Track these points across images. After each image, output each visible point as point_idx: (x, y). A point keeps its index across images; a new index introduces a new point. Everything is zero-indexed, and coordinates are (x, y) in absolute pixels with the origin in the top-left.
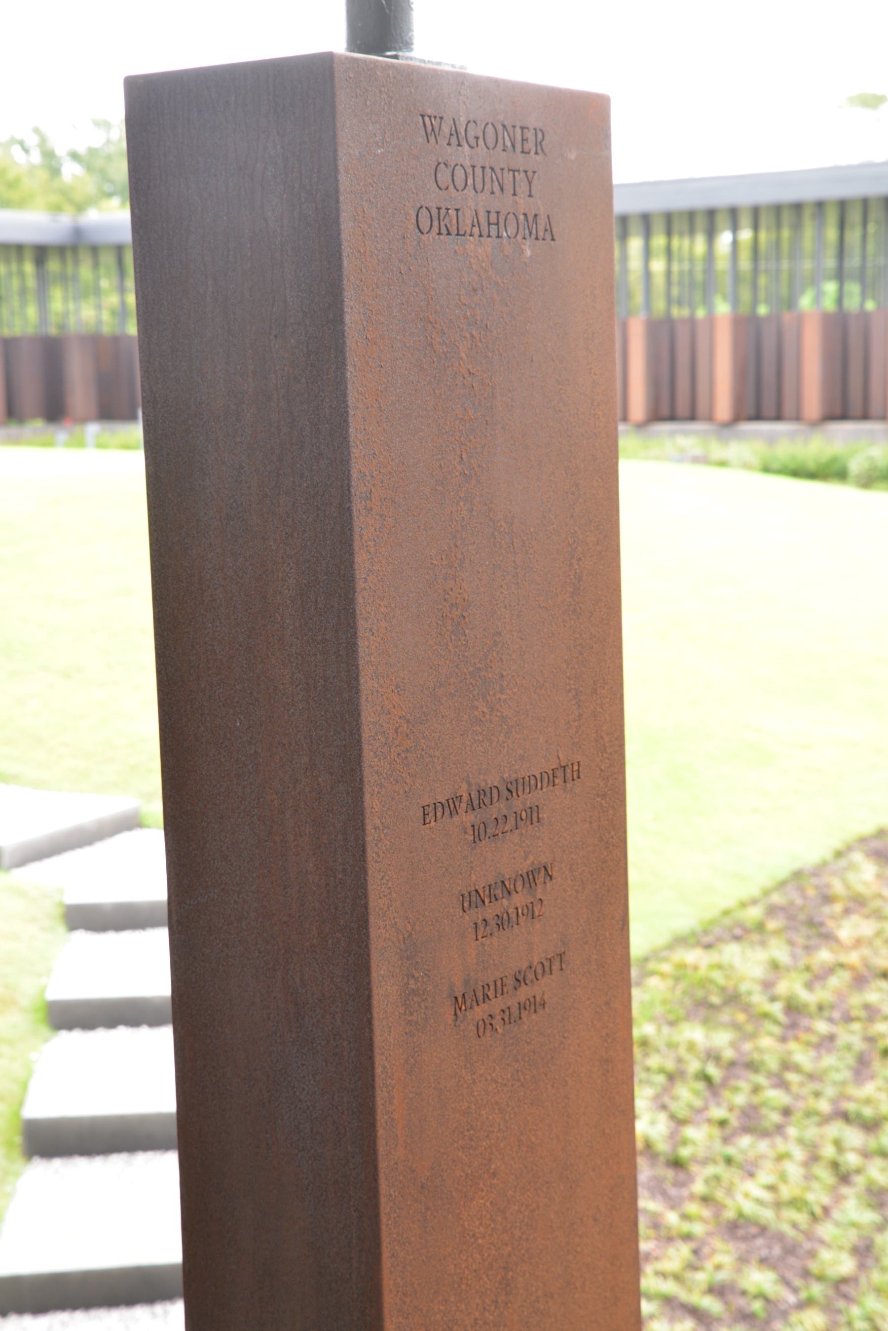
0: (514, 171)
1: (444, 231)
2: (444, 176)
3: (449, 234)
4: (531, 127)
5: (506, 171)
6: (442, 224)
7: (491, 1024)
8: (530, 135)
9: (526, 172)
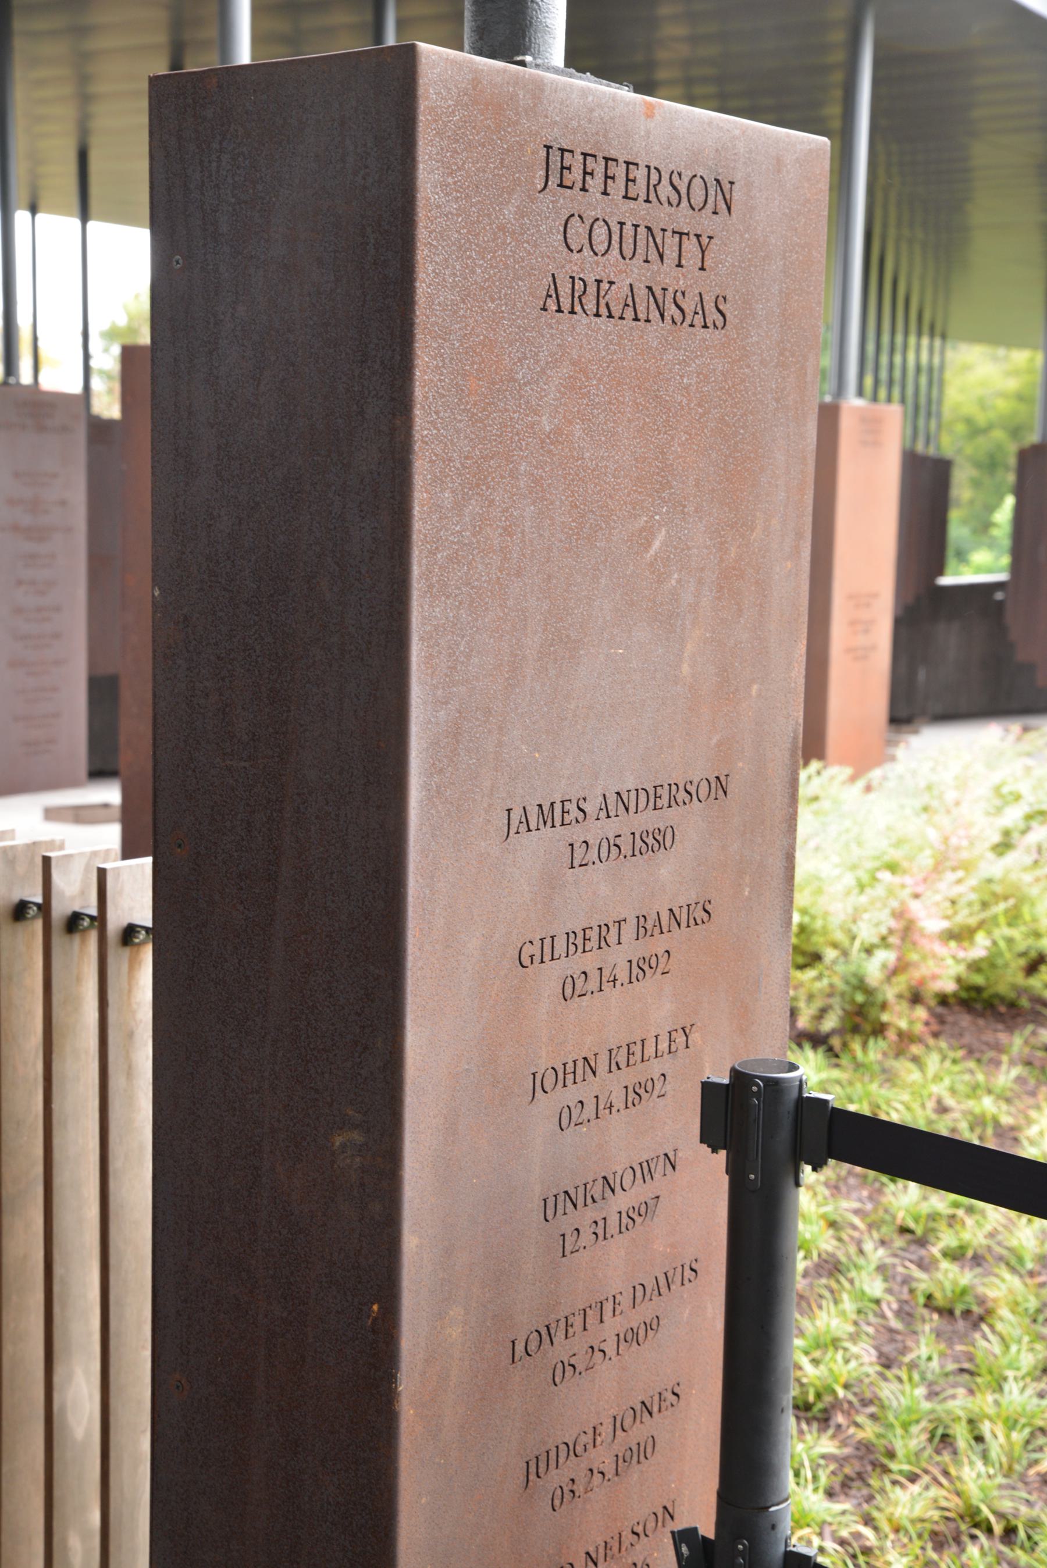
0: (681, 234)
1: (603, 311)
2: (578, 231)
3: (610, 316)
4: (642, 165)
5: (668, 234)
6: (602, 302)
7: (572, 1491)
8: (640, 174)
9: (698, 236)
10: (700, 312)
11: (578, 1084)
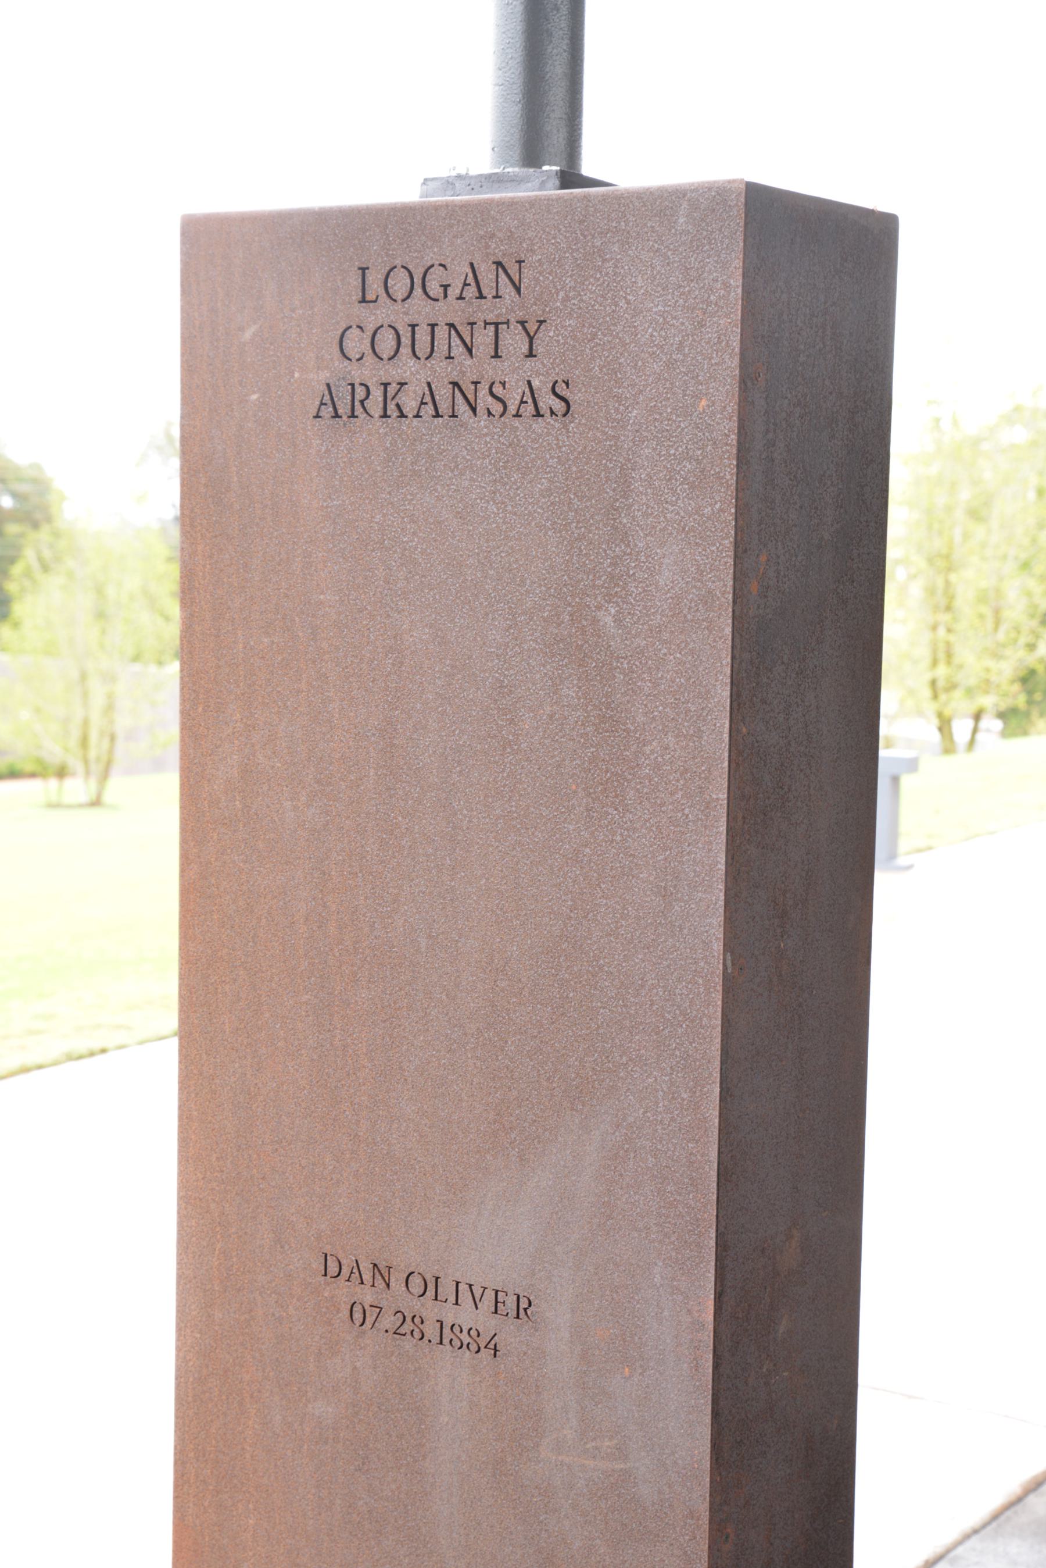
9: (522, 323)
10: (530, 401)
11: (427, 321)
